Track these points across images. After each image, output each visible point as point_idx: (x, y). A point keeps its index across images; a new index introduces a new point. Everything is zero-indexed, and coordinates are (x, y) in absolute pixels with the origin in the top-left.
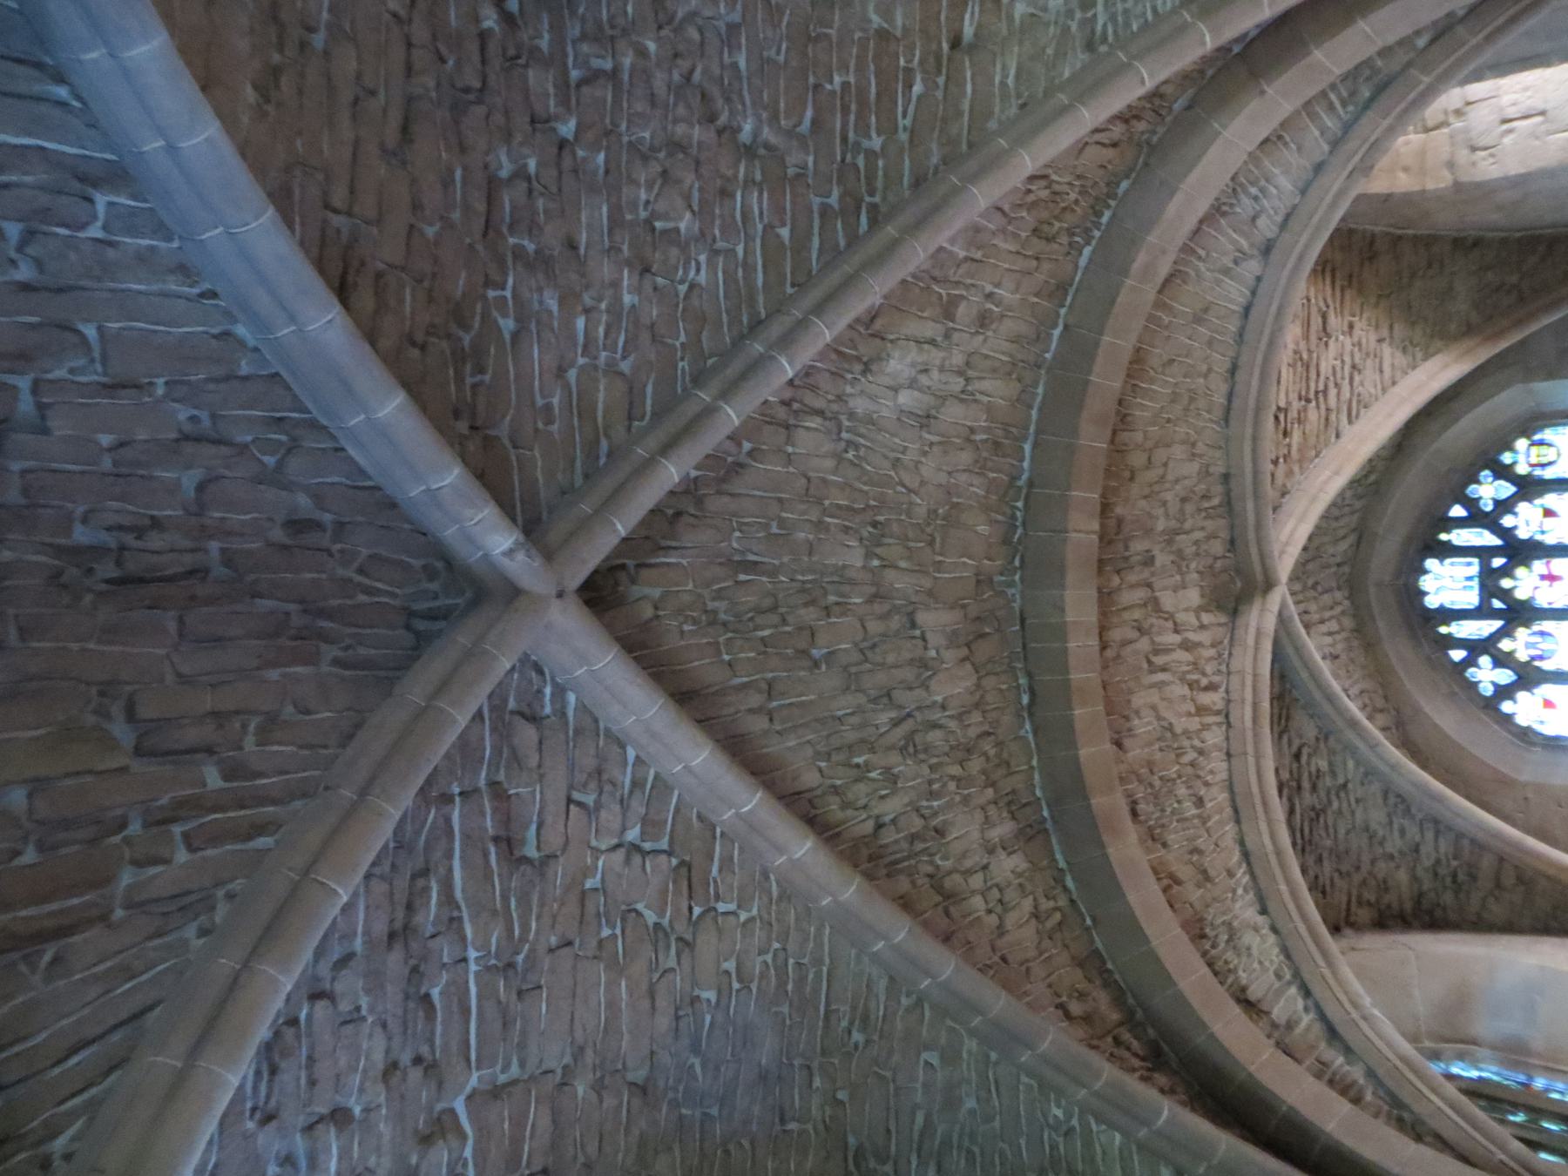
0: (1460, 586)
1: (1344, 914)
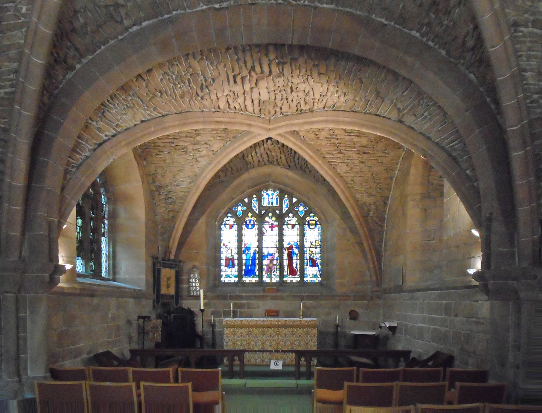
0: (270, 200)
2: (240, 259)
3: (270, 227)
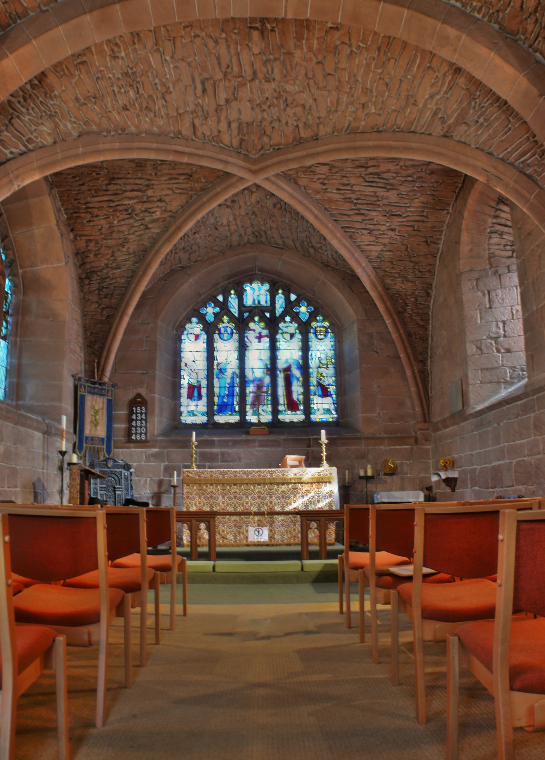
0: (256, 298)
1: (80, 233)
2: (210, 387)
3: (257, 337)
